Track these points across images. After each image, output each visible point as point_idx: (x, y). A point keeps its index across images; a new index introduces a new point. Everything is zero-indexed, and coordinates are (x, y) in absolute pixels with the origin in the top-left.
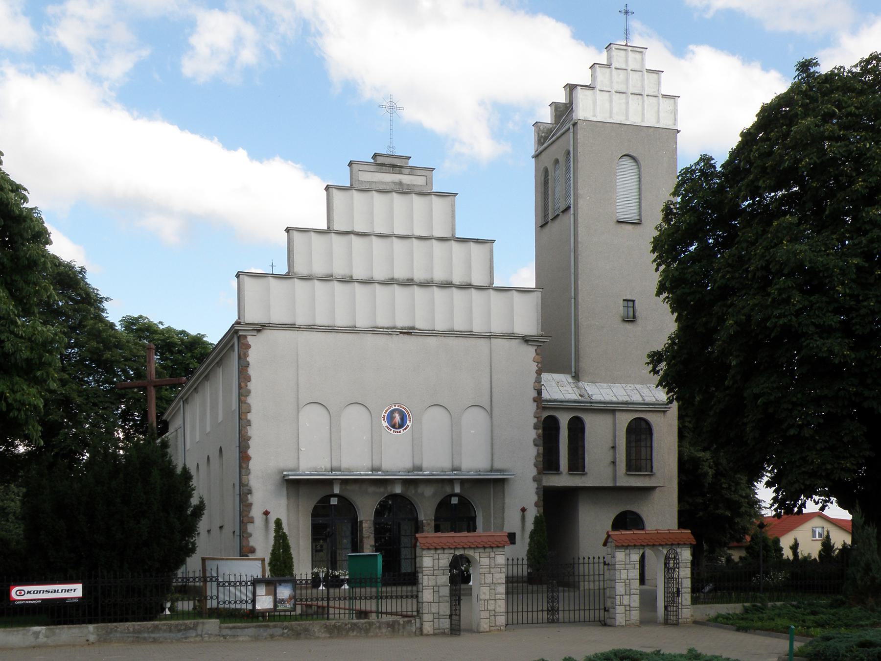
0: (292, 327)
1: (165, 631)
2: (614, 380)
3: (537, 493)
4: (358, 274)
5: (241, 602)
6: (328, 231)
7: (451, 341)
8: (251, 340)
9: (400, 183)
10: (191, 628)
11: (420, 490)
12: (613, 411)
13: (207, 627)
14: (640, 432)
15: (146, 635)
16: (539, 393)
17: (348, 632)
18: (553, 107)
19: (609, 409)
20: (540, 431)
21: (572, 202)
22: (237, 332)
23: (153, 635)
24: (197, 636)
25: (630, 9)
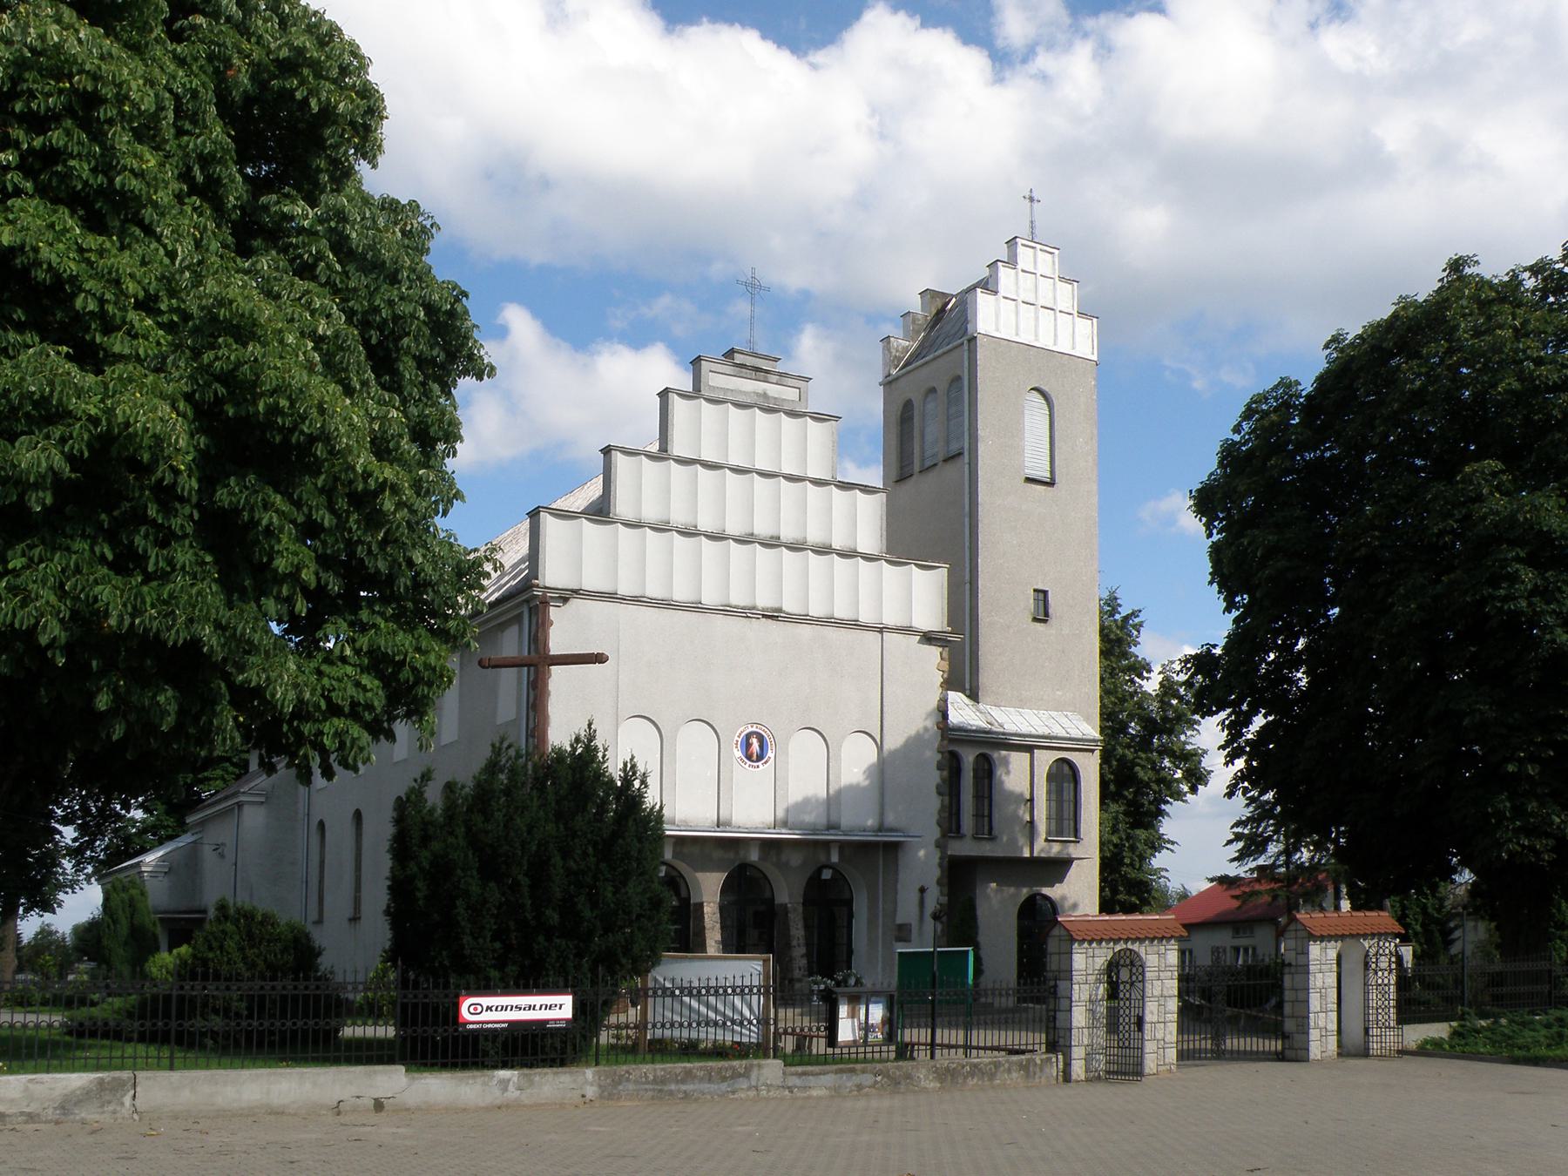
0: (611, 597)
1: (701, 1080)
2: (1022, 703)
3: (940, 865)
4: (705, 524)
5: (672, 1025)
7: (830, 633)
9: (765, 395)
10: (740, 1075)
11: (784, 858)
13: (765, 1071)
14: (1064, 776)
15: (673, 1087)
16: (945, 715)
17: (965, 1078)
19: (1027, 747)
20: (945, 773)
21: (966, 446)
23: (683, 1087)
24: (749, 1088)
25: (1036, 196)
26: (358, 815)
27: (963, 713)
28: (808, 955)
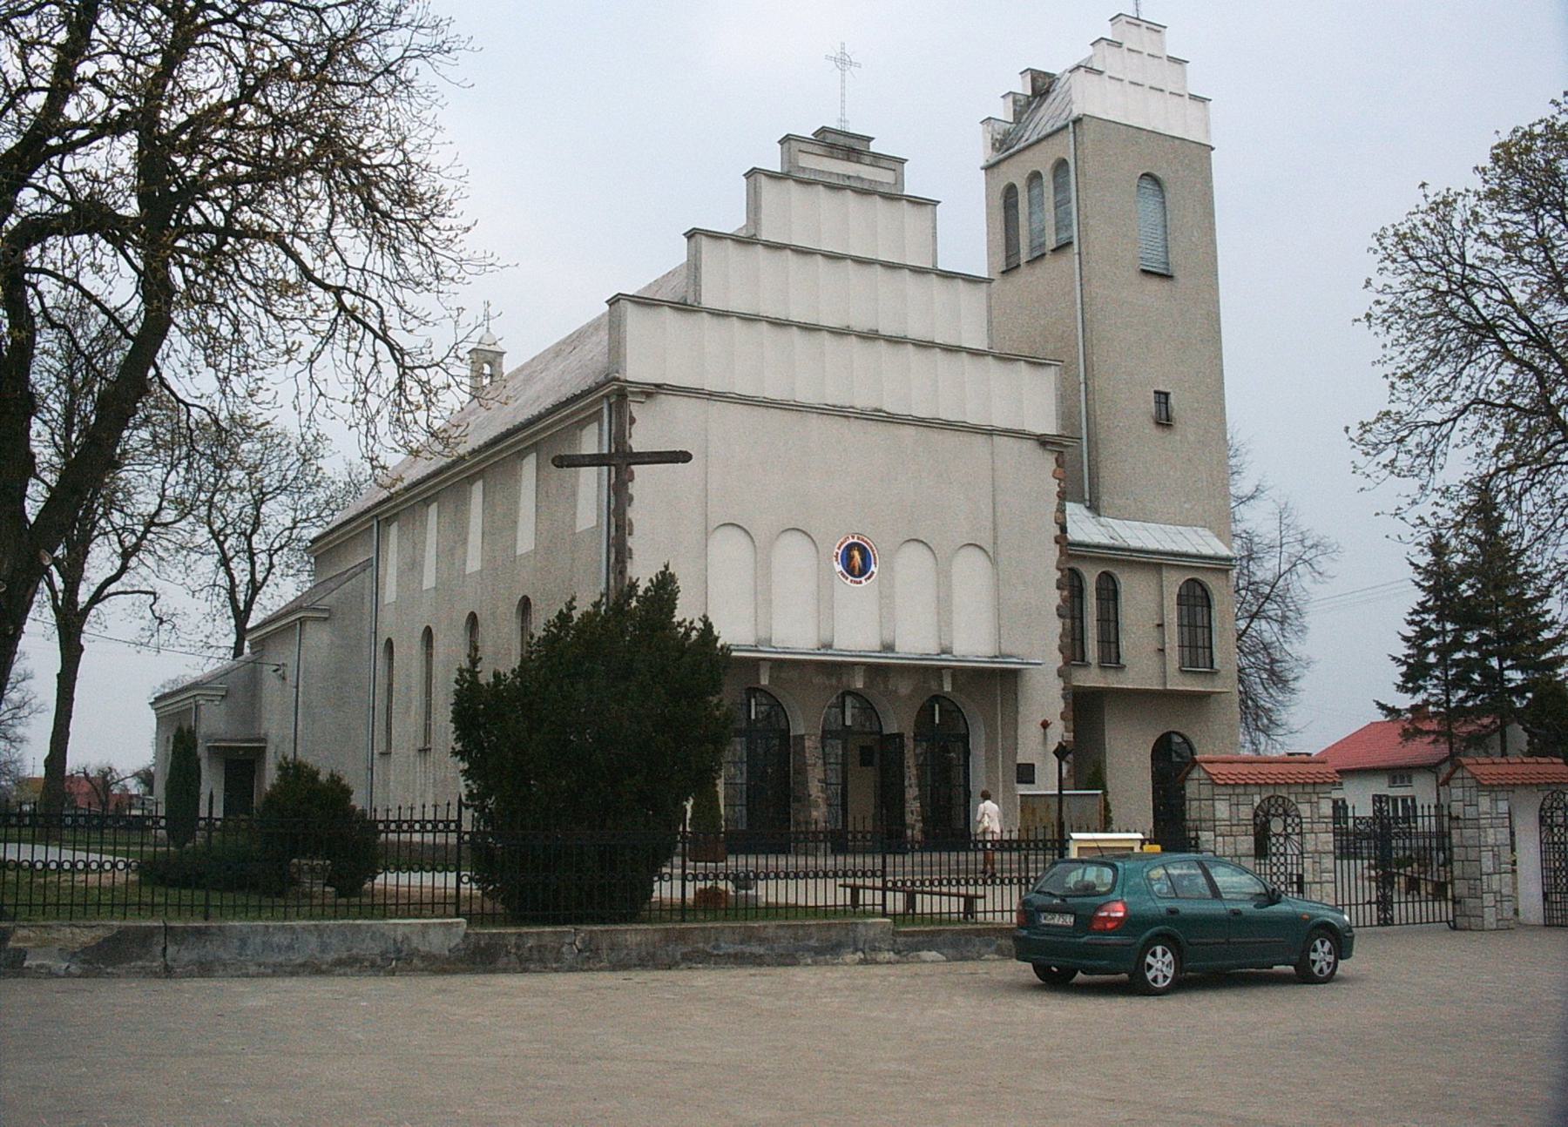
3: (1064, 697)
6: (746, 241)
8: (635, 409)
12: (1158, 567)
16: (1063, 529)
18: (1010, 99)
22: (613, 397)
26: (428, 634)
27: (1084, 528)
28: (920, 797)
